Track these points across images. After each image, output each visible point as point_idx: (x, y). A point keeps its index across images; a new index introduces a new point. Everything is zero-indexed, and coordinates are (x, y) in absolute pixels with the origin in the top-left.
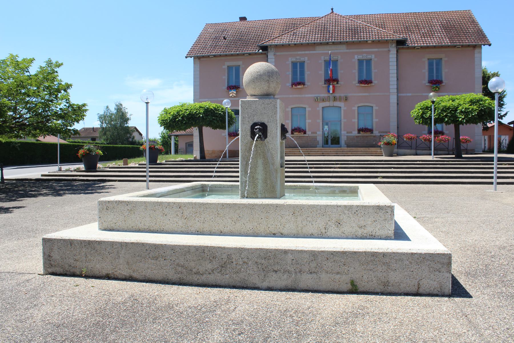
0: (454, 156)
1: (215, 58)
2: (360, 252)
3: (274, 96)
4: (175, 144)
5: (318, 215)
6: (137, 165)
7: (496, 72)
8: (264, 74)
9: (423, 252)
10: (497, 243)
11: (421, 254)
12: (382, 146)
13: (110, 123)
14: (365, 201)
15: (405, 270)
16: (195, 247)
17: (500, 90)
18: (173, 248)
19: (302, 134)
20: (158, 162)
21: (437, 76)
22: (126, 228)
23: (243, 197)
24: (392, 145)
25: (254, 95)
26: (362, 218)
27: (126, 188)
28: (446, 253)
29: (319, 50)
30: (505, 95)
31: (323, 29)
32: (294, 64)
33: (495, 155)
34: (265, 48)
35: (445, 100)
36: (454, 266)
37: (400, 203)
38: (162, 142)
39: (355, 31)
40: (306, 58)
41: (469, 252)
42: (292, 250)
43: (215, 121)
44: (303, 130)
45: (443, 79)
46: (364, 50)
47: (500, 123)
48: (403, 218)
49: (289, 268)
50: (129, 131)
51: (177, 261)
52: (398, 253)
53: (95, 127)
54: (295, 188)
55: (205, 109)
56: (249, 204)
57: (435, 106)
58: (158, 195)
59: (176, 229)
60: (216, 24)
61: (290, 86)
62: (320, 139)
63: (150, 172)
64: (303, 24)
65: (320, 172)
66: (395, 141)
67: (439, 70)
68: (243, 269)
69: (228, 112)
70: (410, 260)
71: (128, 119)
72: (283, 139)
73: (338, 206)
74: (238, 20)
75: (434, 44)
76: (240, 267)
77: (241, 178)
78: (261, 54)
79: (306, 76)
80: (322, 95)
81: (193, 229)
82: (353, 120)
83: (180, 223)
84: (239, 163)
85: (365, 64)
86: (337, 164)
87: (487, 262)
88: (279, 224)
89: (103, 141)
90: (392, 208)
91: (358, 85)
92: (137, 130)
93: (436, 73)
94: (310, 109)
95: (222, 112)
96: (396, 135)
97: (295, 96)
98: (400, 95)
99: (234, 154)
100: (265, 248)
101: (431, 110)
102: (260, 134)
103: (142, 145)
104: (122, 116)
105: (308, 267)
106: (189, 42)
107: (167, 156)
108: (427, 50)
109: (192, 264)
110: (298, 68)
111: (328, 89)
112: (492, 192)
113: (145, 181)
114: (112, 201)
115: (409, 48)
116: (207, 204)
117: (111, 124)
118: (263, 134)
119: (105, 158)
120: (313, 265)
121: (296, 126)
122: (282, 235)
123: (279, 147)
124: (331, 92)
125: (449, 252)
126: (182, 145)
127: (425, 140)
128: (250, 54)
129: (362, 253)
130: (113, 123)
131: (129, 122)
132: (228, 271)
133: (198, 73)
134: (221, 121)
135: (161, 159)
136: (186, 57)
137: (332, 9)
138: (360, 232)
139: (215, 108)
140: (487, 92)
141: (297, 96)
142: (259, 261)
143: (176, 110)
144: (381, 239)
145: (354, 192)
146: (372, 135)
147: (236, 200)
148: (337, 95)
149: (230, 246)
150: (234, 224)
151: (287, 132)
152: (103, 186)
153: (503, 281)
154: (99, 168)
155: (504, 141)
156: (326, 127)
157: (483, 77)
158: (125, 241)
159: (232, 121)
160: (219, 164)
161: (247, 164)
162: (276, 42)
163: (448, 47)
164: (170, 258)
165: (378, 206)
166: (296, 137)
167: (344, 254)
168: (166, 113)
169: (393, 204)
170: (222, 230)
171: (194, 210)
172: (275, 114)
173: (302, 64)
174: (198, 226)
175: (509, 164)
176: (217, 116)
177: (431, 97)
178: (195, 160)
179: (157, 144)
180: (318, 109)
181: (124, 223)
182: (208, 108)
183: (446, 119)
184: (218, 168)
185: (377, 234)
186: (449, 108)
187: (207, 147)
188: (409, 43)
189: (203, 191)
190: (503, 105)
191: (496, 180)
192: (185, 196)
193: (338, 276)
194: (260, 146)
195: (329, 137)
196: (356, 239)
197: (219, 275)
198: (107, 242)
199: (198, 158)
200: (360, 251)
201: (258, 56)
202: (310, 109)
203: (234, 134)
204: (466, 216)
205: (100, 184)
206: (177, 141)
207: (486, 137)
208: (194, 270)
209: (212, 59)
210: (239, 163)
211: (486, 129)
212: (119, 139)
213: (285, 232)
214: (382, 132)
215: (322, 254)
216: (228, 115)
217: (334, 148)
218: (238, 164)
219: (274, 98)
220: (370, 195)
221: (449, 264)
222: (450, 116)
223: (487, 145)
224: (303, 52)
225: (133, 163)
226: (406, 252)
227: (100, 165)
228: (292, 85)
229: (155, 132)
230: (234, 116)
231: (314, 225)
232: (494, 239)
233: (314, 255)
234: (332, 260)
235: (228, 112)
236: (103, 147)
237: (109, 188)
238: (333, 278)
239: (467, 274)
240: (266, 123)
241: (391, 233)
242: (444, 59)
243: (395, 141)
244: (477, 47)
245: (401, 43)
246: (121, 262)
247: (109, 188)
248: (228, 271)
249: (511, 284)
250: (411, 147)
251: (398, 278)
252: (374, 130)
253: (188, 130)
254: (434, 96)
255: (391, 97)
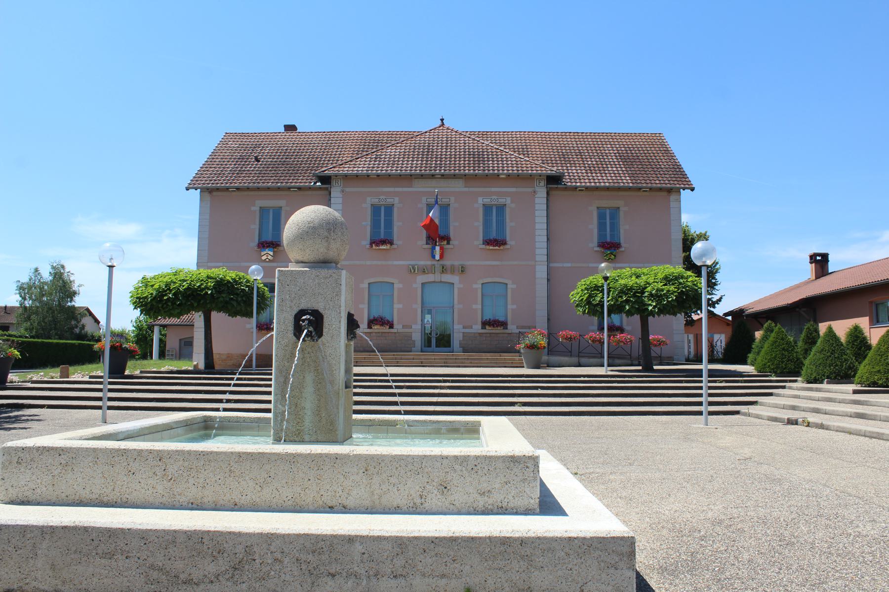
0: (640, 368)
1: (238, 193)
2: (480, 538)
3: (336, 263)
4: (161, 341)
5: (409, 474)
6: (87, 379)
7: (703, 232)
8: (321, 226)
9: (588, 535)
10: (710, 515)
11: (584, 538)
12: (522, 351)
13: (39, 299)
14: (489, 449)
15: (559, 566)
16: (185, 532)
17: (709, 263)
18: (144, 536)
19: (386, 329)
20: (127, 373)
21: (612, 236)
22: (54, 499)
23: (277, 440)
24: (538, 348)
25: (302, 262)
26: (484, 478)
27: (62, 421)
28: (626, 535)
29: (419, 187)
30: (718, 269)
31: (427, 152)
32: (376, 209)
33: (705, 366)
34: (326, 180)
35: (625, 276)
36: (640, 557)
37: (552, 450)
38: (137, 336)
39: (478, 157)
40: (397, 200)
41: (665, 532)
42: (362, 537)
43: (235, 304)
44: (388, 321)
45: (622, 241)
46: (493, 189)
47: (711, 315)
48: (554, 474)
49: (356, 569)
50: (74, 314)
51: (151, 560)
52: (545, 538)
53: (9, 305)
54: (370, 424)
55: (217, 281)
56: (287, 454)
57: (609, 284)
58: (121, 437)
59: (151, 499)
60: (242, 134)
61: (368, 246)
62: (417, 337)
63: (110, 390)
64: (393, 142)
65: (416, 398)
66: (543, 342)
67: (614, 227)
68: (273, 573)
69: (258, 288)
70: (567, 550)
71: (75, 293)
72: (351, 340)
73: (443, 457)
74: (283, 130)
75: (607, 184)
76: (268, 568)
77: (275, 407)
78: (320, 188)
79: (395, 229)
80: (422, 263)
81: (183, 500)
82: (474, 306)
83: (160, 489)
84: (273, 377)
85: (494, 213)
86: (445, 381)
87: (694, 547)
88: (340, 490)
89: (22, 331)
90: (535, 460)
91: (484, 246)
92: (91, 314)
93: (611, 231)
94: (401, 286)
95: (247, 286)
96: (546, 332)
97: (375, 263)
98: (551, 265)
99: (264, 361)
100: (314, 532)
101: (602, 291)
102: (311, 329)
103: (99, 340)
104: (62, 286)
105: (391, 566)
106: (194, 160)
107: (145, 362)
108: (596, 193)
109: (179, 565)
110: (382, 215)
111: (432, 252)
112: (702, 428)
113: (99, 408)
114: (30, 448)
115: (567, 188)
116: (211, 453)
117: (41, 302)
118: (315, 329)
119: (27, 363)
120: (399, 562)
121: (375, 314)
122: (345, 510)
123: (343, 353)
124: (437, 257)
125: (631, 534)
126: (172, 343)
127: (593, 341)
128: (300, 188)
129: (485, 538)
130: (45, 299)
131: (76, 298)
132: (245, 578)
133: (208, 217)
134: (245, 302)
135: (133, 368)
136: (187, 189)
137: (442, 120)
138: (481, 502)
139: (234, 280)
140: (689, 264)
141: (379, 263)
142: (303, 557)
143: (165, 280)
144: (517, 513)
145: (473, 431)
146: (506, 331)
147: (264, 445)
148: (447, 263)
149: (251, 531)
150: (260, 489)
151: (358, 326)
152: (17, 416)
153: (720, 580)
154: (12, 382)
155: (719, 343)
156: (428, 318)
157: (683, 239)
158: (51, 524)
159: (264, 303)
160: (238, 379)
161: (286, 381)
162: (346, 170)
163: (630, 189)
164: (138, 555)
165: (512, 457)
166: (376, 335)
167: (453, 541)
168: (146, 286)
169: (538, 452)
170: (237, 500)
171: (186, 464)
172: (337, 295)
173: (389, 209)
174: (193, 493)
175: (727, 381)
176: (237, 294)
177: (603, 270)
178: (196, 371)
179: (127, 340)
180: (414, 286)
181: (51, 489)
182: (221, 279)
183: (627, 307)
184: (235, 385)
185: (511, 505)
186: (631, 289)
187: (218, 348)
188: (566, 179)
189: (206, 428)
190: (715, 284)
191: (706, 408)
192: (171, 439)
193: (444, 581)
194: (309, 350)
195: (433, 335)
196: (475, 514)
197: (229, 584)
198: (13, 526)
199: (202, 366)
200: (481, 535)
201: (314, 192)
202: (401, 286)
203: (265, 327)
204: (659, 470)
205: (11, 412)
206: (165, 335)
207: (691, 337)
208: (182, 576)
209: (234, 193)
210: (273, 377)
211: (690, 323)
212: (55, 329)
213: (350, 503)
214: (523, 327)
215: (415, 542)
216: (258, 292)
217: (443, 354)
218: (270, 380)
219: (337, 268)
220: (500, 436)
221: (632, 554)
222: (633, 301)
223: (692, 350)
224: (392, 189)
225: (79, 374)
226: (559, 535)
227: (13, 377)
228: (371, 244)
229: (125, 319)
230: (268, 294)
231: (402, 489)
232: (705, 508)
233: (401, 544)
234: (433, 553)
235: (258, 288)
236: (23, 342)
237: (28, 420)
238: (434, 586)
239: (663, 570)
240: (321, 311)
241: (534, 502)
242: (623, 209)
243: (543, 342)
244: (672, 191)
245: (554, 180)
246: (39, 566)
247: (28, 420)
248: (245, 578)
249: (732, 585)
250: (570, 353)
251: (547, 583)
252: (509, 323)
253: (185, 317)
254: (607, 268)
255: (538, 268)
